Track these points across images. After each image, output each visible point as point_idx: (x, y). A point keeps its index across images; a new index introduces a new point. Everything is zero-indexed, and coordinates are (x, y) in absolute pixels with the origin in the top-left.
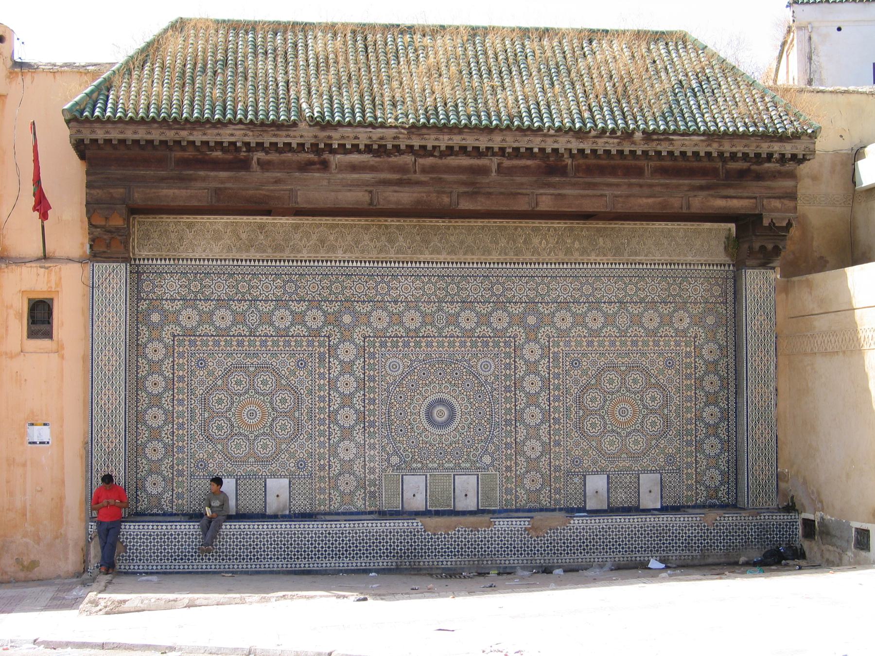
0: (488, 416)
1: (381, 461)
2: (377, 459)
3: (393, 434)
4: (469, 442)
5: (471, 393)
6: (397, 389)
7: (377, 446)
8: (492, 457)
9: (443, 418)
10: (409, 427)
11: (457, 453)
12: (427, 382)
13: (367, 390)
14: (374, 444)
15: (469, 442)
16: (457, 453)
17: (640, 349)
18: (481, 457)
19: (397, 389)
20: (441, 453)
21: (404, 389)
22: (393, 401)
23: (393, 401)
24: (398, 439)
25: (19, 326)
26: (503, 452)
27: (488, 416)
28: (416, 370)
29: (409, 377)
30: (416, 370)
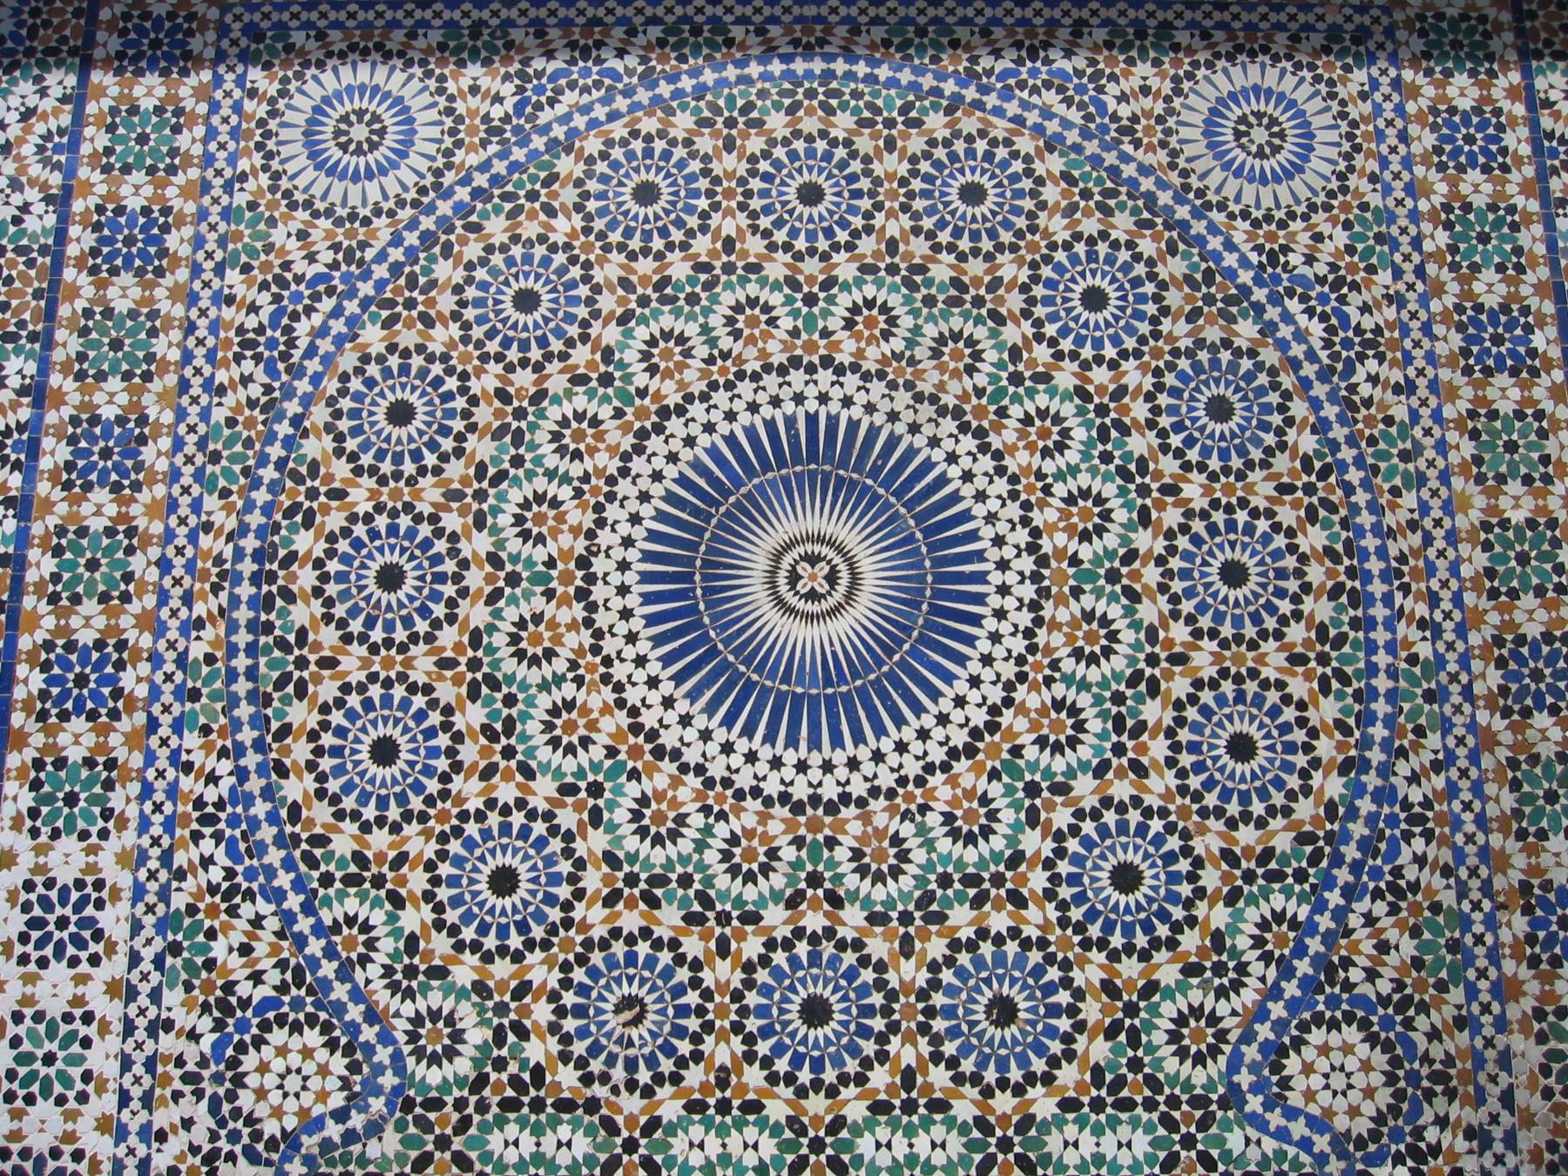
0: (1321, 609)
1: (138, 1082)
2: (102, 1058)
3: (295, 788)
4: (1126, 878)
5: (1133, 375)
6: (373, 337)
7: (113, 920)
8: (1397, 1051)
9: (840, 627)
10: (474, 715)
11: (1003, 1011)
12: (679, 269)
13: (68, 343)
14: (93, 891)
15: (1126, 878)
16: (1003, 1011)
17: (124, 991)
18: (1276, 1053)
19: (373, 337)
20: (815, 1012)
21: (440, 337)
22: (315, 447)
23: (315, 447)
24: (343, 844)
25: (8, 823)
26: (1506, 990)
27: (1321, 609)
28: (566, 165)
29: (497, 228)
30: (566, 165)
